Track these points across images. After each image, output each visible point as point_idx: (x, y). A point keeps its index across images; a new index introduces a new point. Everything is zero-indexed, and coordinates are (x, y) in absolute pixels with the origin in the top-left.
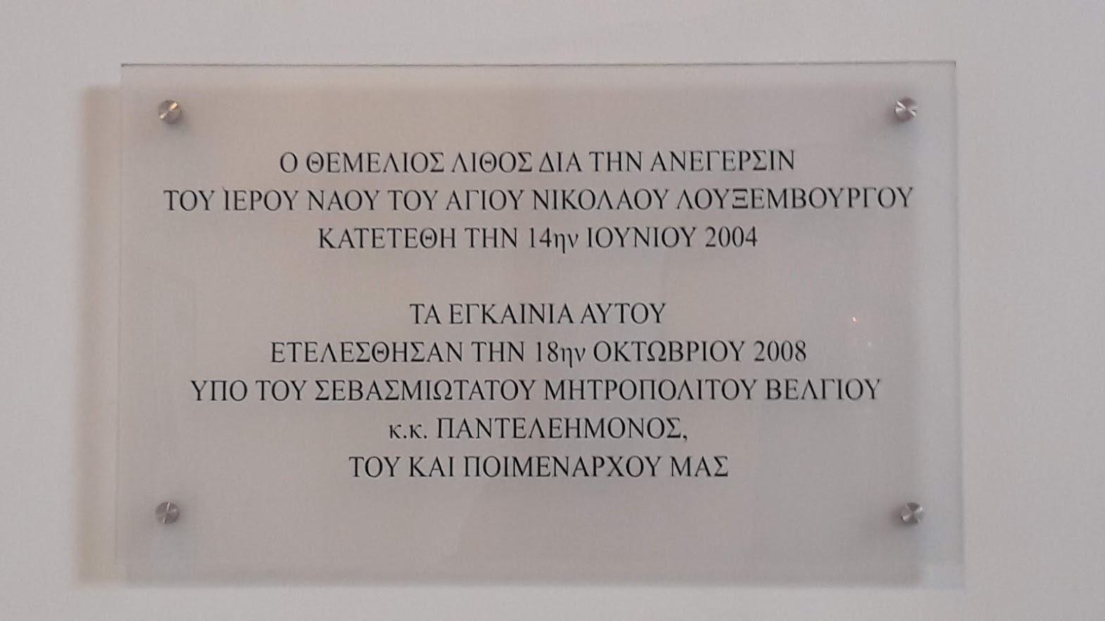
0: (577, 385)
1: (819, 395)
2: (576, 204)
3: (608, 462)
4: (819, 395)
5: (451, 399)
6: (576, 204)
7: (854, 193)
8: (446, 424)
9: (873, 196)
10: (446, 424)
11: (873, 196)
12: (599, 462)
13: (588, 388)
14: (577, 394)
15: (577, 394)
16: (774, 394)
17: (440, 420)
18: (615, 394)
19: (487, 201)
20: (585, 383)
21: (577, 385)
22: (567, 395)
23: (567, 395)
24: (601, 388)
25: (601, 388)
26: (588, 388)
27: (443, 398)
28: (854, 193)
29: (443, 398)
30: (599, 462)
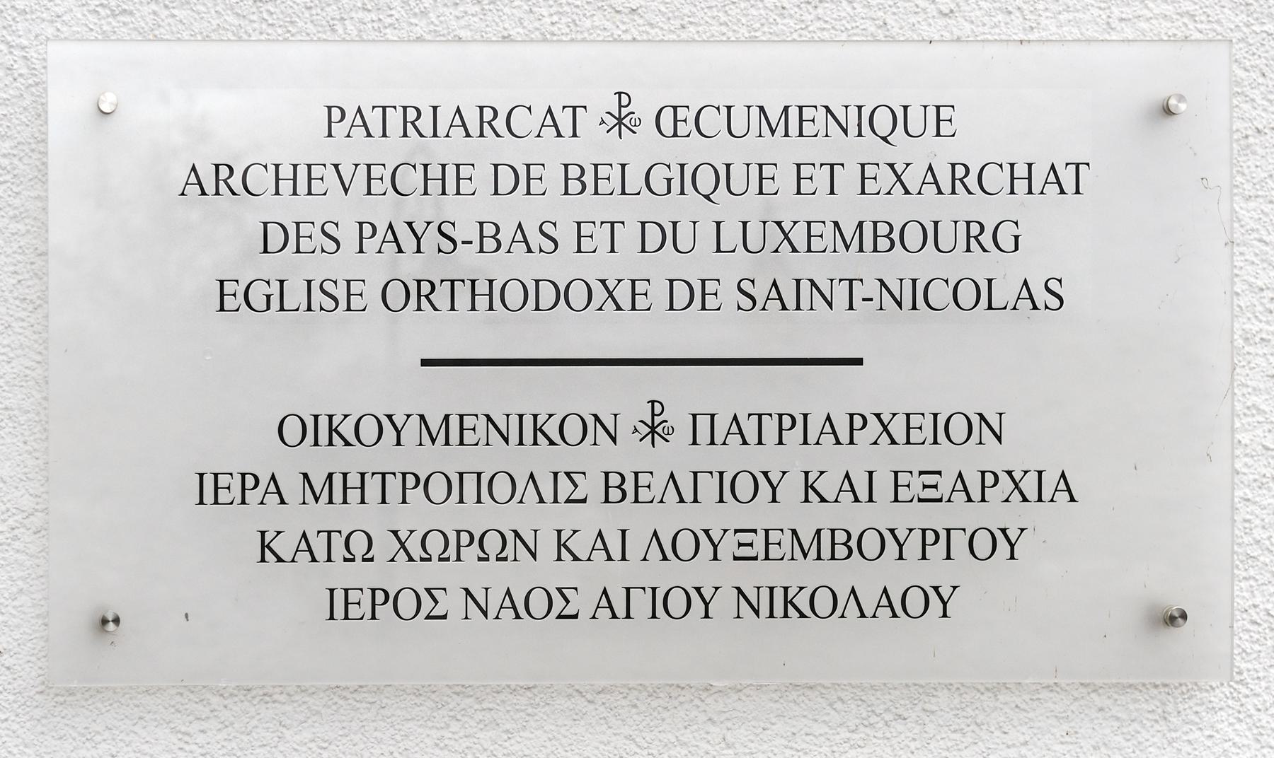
0: (354, 480)
1: (688, 496)
2: (556, 437)
3: (873, 421)
4: (688, 496)
5: (371, 560)
6: (556, 437)
7: (930, 537)
8: (703, 423)
9: (960, 541)
10: (703, 423)
11: (960, 541)
12: (858, 422)
13: (373, 486)
14: (354, 495)
15: (354, 495)
16: (615, 494)
17: (694, 416)
18: (416, 495)
19: (727, 488)
20: (367, 477)
21: (354, 480)
22: (338, 496)
23: (338, 496)
24: (394, 485)
25: (394, 485)
26: (373, 486)
27: (359, 559)
28: (930, 537)
29: (359, 559)
30: (858, 422)
